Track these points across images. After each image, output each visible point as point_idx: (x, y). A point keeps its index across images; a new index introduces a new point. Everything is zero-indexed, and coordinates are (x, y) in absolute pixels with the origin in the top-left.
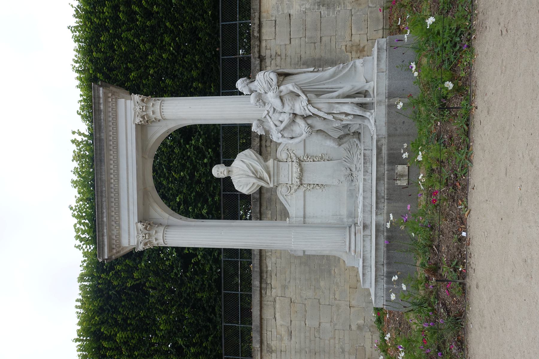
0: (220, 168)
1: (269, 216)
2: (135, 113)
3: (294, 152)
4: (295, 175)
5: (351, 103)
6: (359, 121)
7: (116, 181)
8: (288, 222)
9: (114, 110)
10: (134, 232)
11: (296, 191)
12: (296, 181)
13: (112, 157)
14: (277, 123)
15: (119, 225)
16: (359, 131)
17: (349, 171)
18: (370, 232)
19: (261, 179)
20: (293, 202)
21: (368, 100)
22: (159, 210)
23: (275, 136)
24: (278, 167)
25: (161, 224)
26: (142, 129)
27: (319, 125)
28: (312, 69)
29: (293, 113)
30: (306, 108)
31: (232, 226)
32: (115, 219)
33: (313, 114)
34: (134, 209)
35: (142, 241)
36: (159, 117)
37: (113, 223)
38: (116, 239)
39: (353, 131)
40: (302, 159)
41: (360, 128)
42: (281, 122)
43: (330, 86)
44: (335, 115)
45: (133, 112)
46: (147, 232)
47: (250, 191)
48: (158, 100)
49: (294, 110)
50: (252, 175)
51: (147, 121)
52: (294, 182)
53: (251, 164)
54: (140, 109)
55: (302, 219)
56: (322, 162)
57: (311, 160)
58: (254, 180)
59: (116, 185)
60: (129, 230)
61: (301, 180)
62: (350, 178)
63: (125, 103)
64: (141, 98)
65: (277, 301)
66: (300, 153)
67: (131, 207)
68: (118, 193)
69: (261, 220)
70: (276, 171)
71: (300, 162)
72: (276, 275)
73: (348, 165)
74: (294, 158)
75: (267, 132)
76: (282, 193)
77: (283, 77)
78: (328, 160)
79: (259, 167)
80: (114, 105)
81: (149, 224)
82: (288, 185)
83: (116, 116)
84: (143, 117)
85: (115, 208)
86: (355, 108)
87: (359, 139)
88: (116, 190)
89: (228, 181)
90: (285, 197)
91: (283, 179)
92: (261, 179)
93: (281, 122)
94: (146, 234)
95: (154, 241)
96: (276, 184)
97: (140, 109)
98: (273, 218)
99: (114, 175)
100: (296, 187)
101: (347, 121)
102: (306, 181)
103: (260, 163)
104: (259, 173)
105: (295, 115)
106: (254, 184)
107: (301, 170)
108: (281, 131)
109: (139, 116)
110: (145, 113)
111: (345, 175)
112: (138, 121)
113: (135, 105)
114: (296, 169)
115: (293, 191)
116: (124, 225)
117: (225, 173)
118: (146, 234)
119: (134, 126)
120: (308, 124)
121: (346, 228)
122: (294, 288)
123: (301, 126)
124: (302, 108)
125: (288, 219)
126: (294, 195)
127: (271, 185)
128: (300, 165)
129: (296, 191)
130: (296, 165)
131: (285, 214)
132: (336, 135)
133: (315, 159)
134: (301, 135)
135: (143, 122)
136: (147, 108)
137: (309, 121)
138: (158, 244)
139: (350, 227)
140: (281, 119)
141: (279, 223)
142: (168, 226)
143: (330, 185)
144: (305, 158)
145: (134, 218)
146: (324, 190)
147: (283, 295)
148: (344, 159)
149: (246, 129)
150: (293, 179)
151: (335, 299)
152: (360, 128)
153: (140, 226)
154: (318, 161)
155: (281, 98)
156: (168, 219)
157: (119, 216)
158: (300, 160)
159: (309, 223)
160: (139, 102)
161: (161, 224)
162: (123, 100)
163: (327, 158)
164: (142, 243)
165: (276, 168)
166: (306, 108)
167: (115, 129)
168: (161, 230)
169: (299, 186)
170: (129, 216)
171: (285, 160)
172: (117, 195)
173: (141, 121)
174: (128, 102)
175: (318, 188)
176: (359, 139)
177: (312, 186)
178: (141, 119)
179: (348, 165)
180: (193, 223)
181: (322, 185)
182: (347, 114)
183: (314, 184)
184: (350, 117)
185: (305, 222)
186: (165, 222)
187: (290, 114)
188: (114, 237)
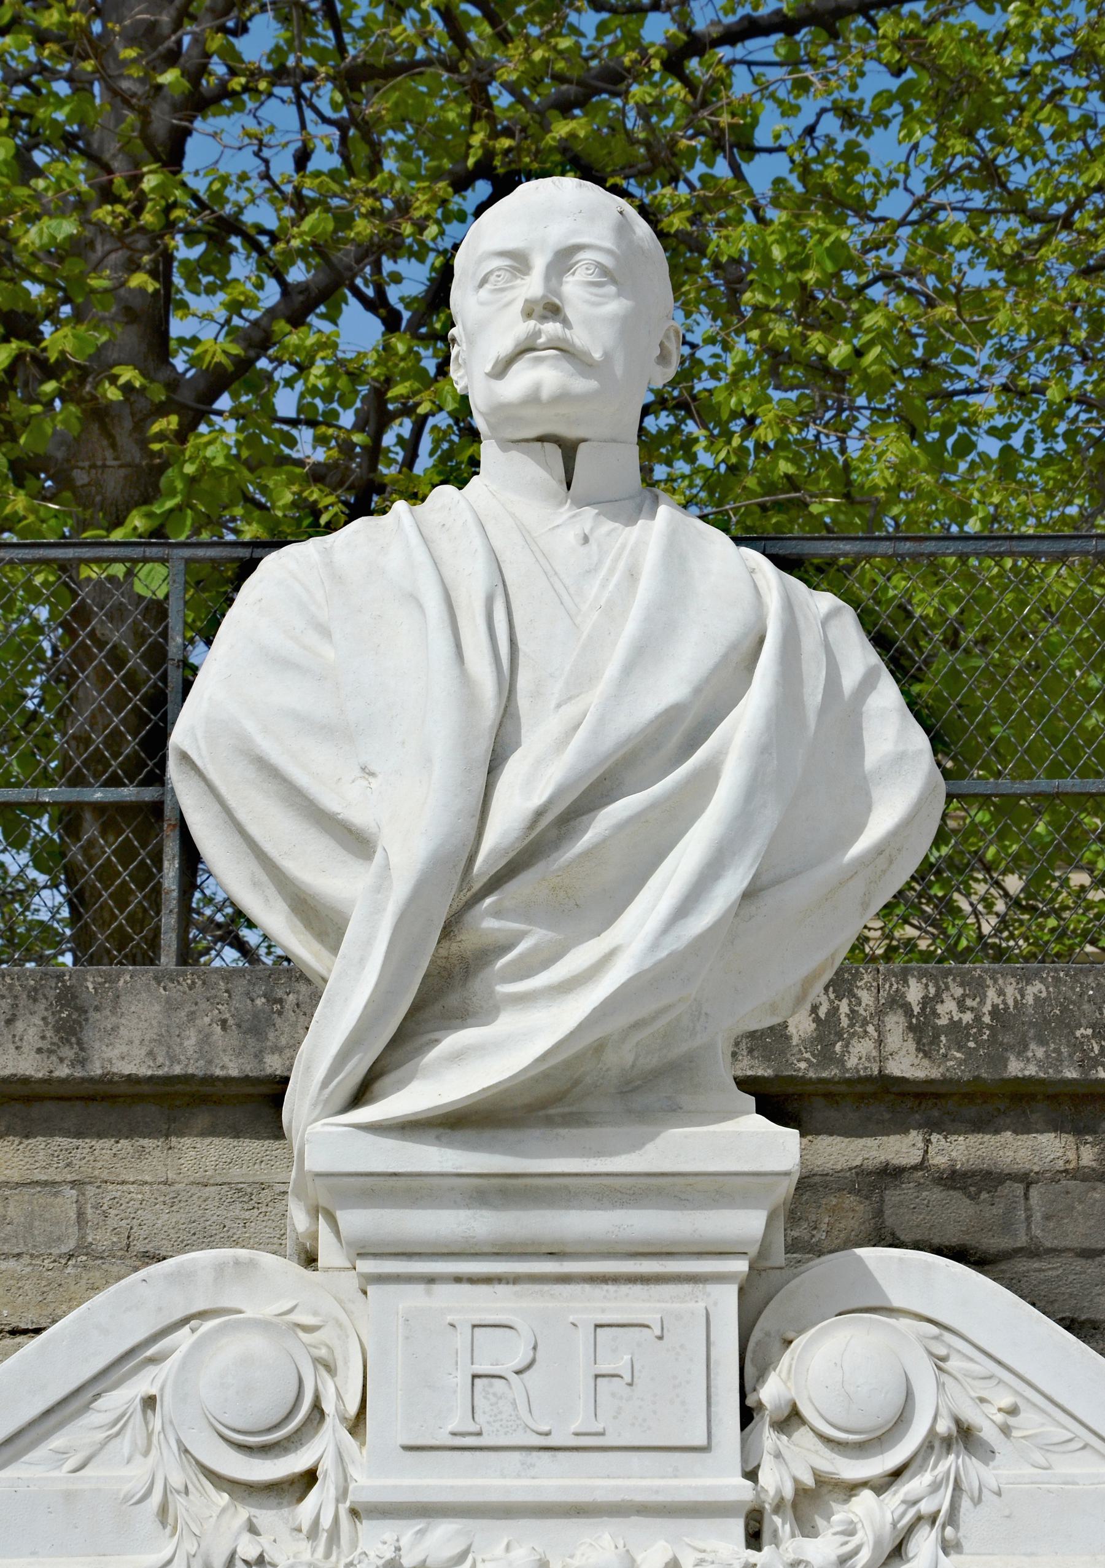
19: (440, 992)
50: (522, 794)
58: (411, 821)
79: (635, 936)
92: (440, 992)
106: (357, 842)
117: (541, 375)
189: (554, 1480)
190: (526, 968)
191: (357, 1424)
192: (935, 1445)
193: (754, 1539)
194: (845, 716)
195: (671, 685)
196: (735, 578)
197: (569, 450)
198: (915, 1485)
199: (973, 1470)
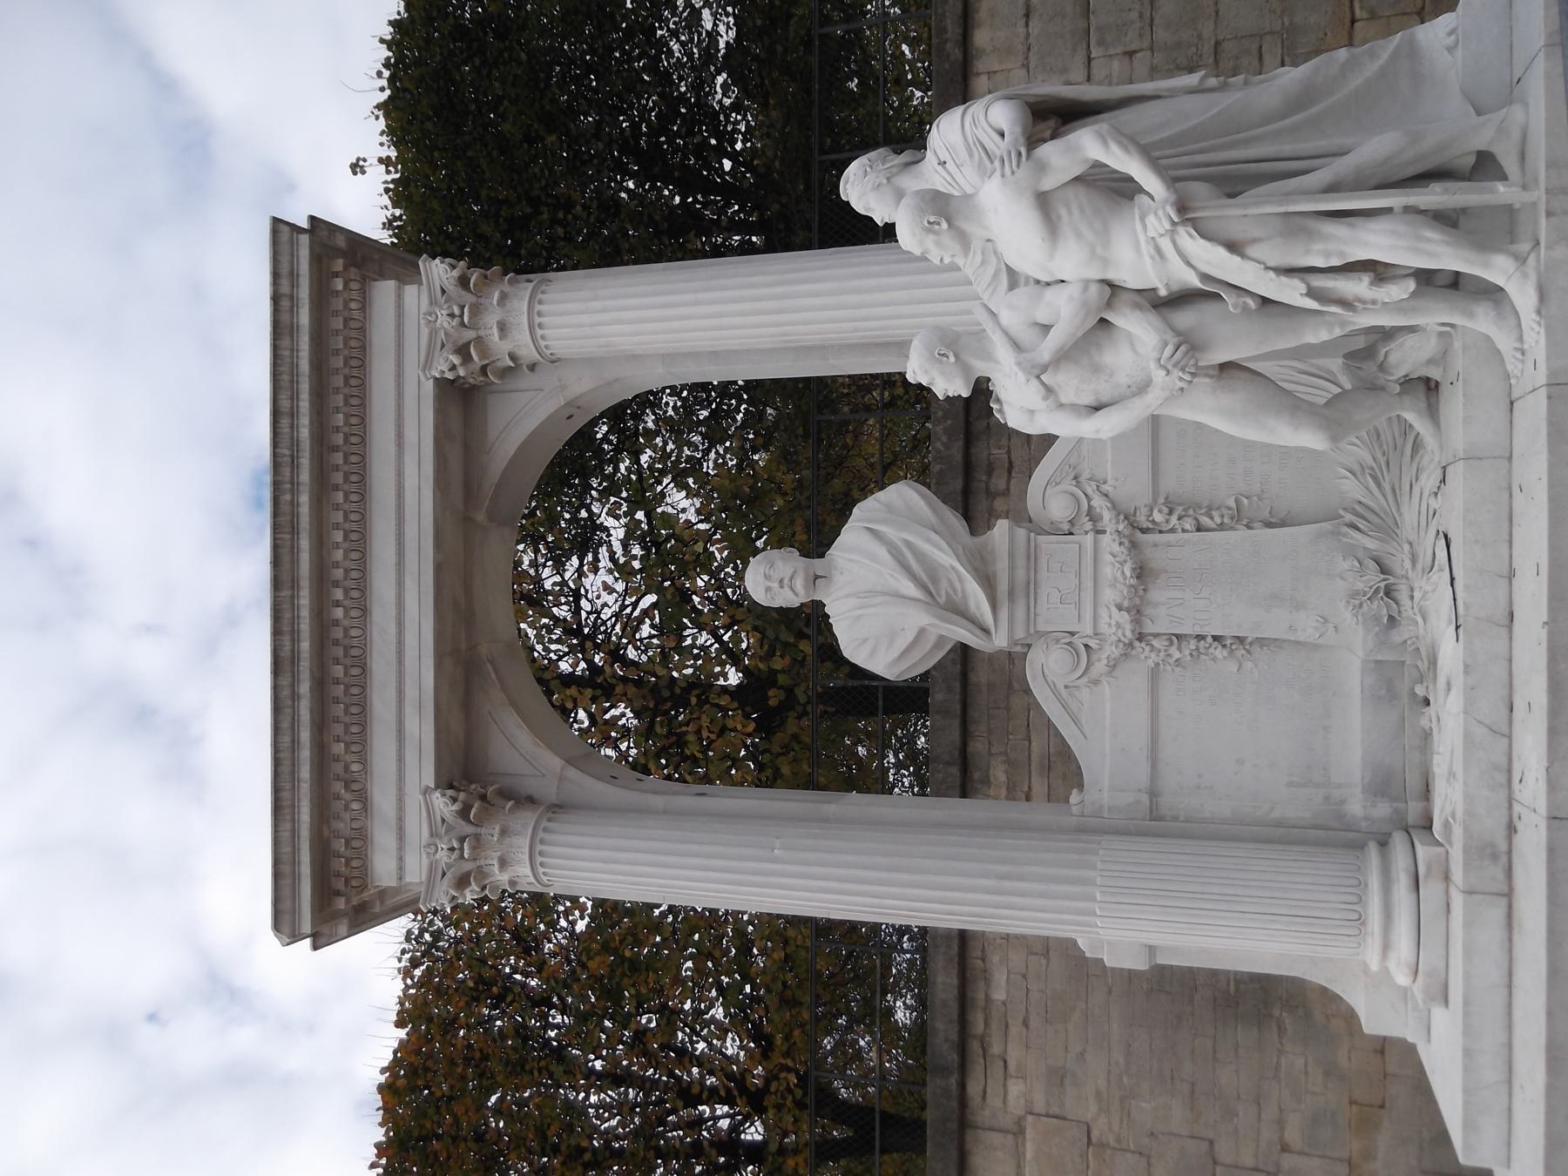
0: (779, 564)
1: (999, 773)
2: (433, 334)
3: (1105, 488)
4: (1109, 595)
5: (1408, 210)
6: (1435, 315)
7: (354, 613)
8: (1075, 809)
9: (353, 324)
10: (417, 828)
11: (1113, 666)
12: (1115, 623)
13: (340, 517)
14: (1026, 336)
15: (364, 798)
16: (1434, 373)
17: (1374, 578)
18: (1501, 875)
20: (1098, 716)
21: (1502, 192)
22: (524, 738)
23: (1020, 407)
24: (1032, 557)
25: (531, 800)
26: (463, 400)
27: (1234, 341)
28: (1193, 79)
29: (1103, 281)
30: (1165, 244)
31: (825, 820)
32: (347, 768)
33: (1205, 277)
34: (421, 730)
35: (449, 866)
36: (528, 352)
37: (338, 787)
38: (349, 853)
39: (1400, 373)
40: (1142, 519)
41: (1442, 358)
42: (1046, 328)
43: (1287, 149)
44: (1320, 282)
45: (425, 331)
46: (470, 829)
47: (904, 666)
48: (529, 281)
49: (1105, 262)
50: (910, 589)
51: (484, 369)
52: (1103, 627)
53: (908, 544)
54: (452, 315)
55: (1145, 798)
56: (1240, 534)
57: (1188, 524)
58: (919, 618)
59: (354, 633)
60: (400, 820)
61: (1137, 613)
62: (1380, 607)
63: (399, 297)
64: (456, 273)
65: (1029, 1133)
66: (1134, 488)
67: (412, 725)
68: (363, 666)
69: (964, 795)
70: (1021, 574)
71: (1136, 529)
72: (1026, 1024)
73: (1371, 544)
74: (1107, 515)
75: (982, 391)
76: (1047, 672)
77: (1052, 123)
78: (1269, 525)
79: (945, 558)
80: (353, 305)
81: (483, 798)
82: (1078, 642)
83: (363, 348)
84: (463, 351)
85: (347, 726)
86: (1429, 234)
87: (1433, 412)
88: (354, 652)
89: (810, 622)
90: (1064, 692)
91: (1054, 612)
92: (958, 610)
93: (1046, 328)
94: (462, 840)
95: (496, 869)
96: (1020, 634)
97: (452, 315)
98: (1018, 791)
99: (346, 591)
100: (1113, 651)
101: (1383, 304)
102: (1161, 621)
103: (951, 539)
104: (944, 584)
105: (1113, 288)
107: (1142, 573)
108: (1045, 368)
109: (449, 346)
110: (470, 335)
111: (1354, 594)
112: (440, 367)
113: (433, 302)
114: (1114, 567)
115: (1100, 667)
116: (383, 798)
117: (799, 584)
118: (462, 840)
119: (429, 386)
120: (1177, 333)
121: (1359, 847)
122: (1102, 1084)
123: (1140, 335)
124: (1147, 250)
125: (1074, 798)
126: (1106, 689)
127: (1000, 641)
128: (1134, 545)
129: (1113, 666)
130: (1116, 548)
131: (1063, 770)
132: (1321, 394)
133: (1205, 520)
134: (1143, 387)
135: (462, 372)
136: (476, 310)
137: (1185, 318)
138: (512, 883)
139: (1383, 844)
140: (1042, 316)
141: (1040, 812)
142: (558, 808)
143: (1276, 642)
144: (1158, 517)
145: (422, 770)
146: (1248, 665)
147: (1055, 1110)
148: (1349, 517)
149: (897, 396)
150: (1104, 613)
151: (1285, 1148)
152: (1442, 358)
153: (442, 805)
154: (1222, 527)
155: (1043, 201)
156: (561, 778)
157: (364, 761)
158: (1134, 526)
159: (1175, 819)
160: (452, 288)
161: (531, 800)
162: (390, 285)
163: (1266, 514)
164: (449, 875)
165: (1021, 561)
166: (1165, 244)
167: (354, 401)
168: (525, 820)
169: (1131, 645)
170: (401, 759)
171: (1066, 527)
172: (355, 671)
173: (453, 368)
174: (410, 291)
175: (1220, 653)
176: (1433, 412)
177: (1193, 644)
178: (455, 360)
179: (1371, 544)
180: (658, 801)
181: (1240, 640)
182: (1378, 271)
183: (1200, 637)
184: (1399, 291)
185: (1157, 822)
186: (546, 789)
187: (1087, 283)
188: (339, 845)
189: (1088, 584)
190: (954, 590)
191: (1072, 634)
192: (1078, 485)
193: (1104, 532)
194: (889, 508)
195: (882, 552)
196: (852, 537)
197: (817, 577)
198: (1089, 491)
199: (1085, 475)
